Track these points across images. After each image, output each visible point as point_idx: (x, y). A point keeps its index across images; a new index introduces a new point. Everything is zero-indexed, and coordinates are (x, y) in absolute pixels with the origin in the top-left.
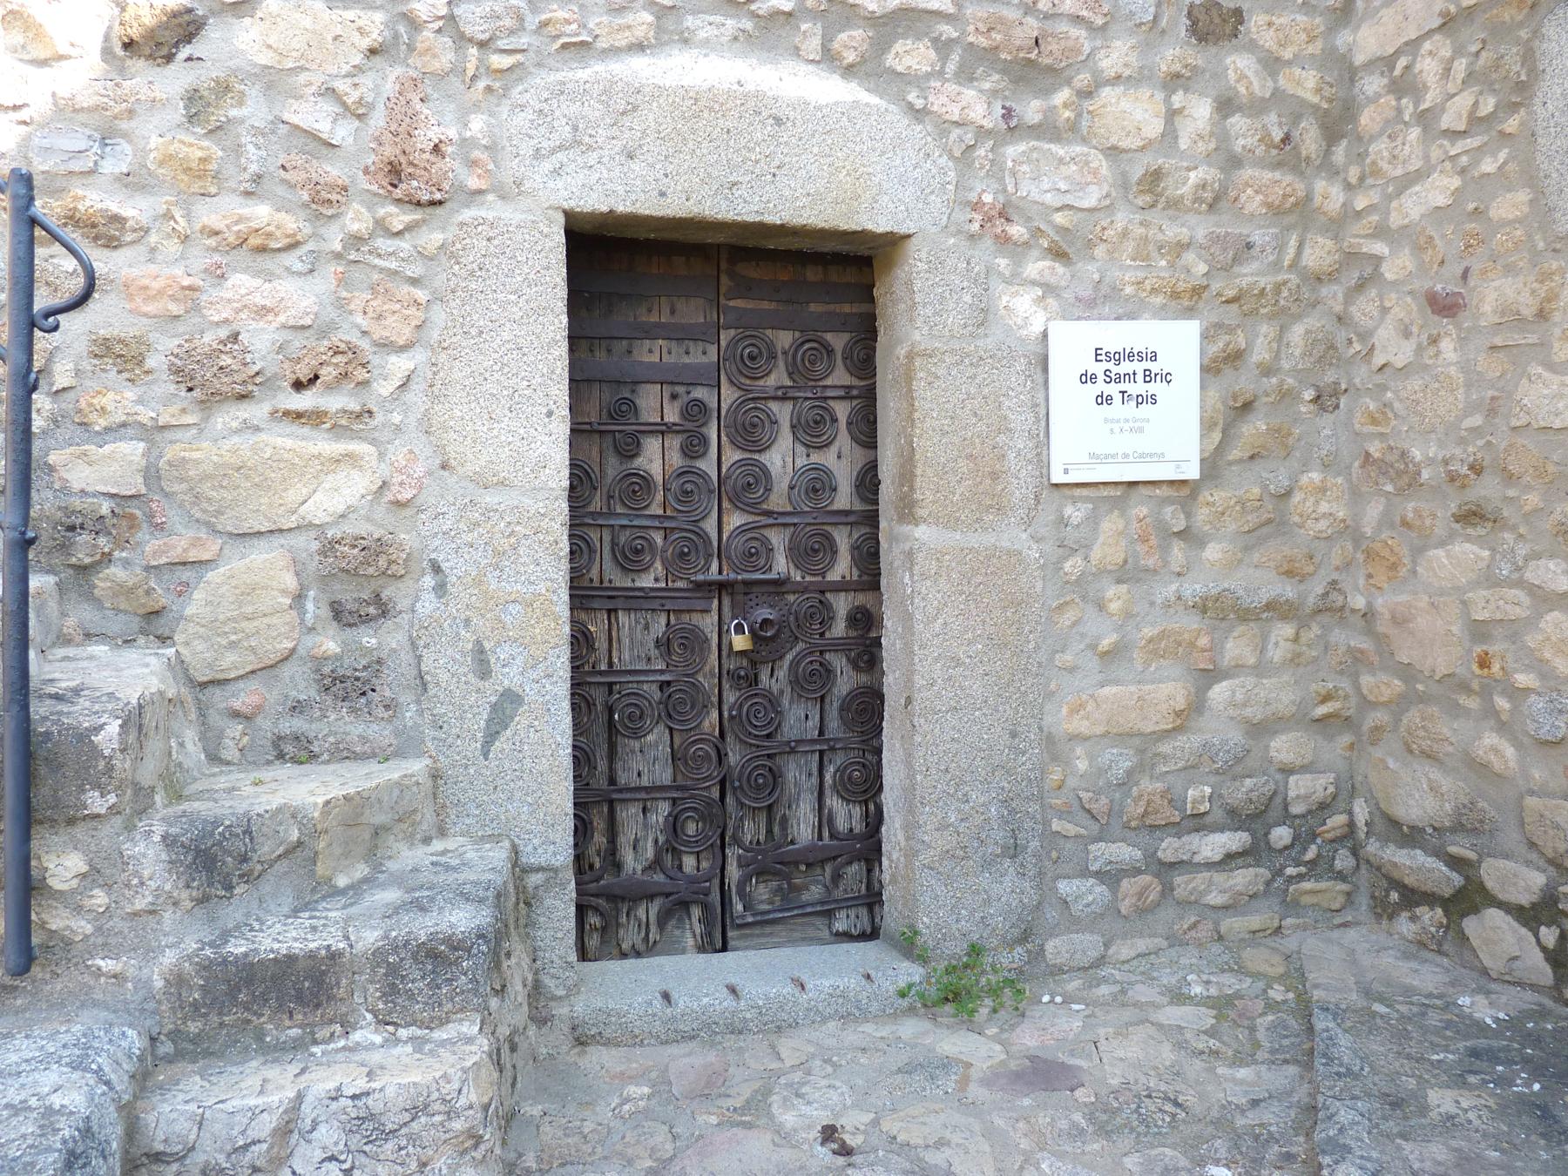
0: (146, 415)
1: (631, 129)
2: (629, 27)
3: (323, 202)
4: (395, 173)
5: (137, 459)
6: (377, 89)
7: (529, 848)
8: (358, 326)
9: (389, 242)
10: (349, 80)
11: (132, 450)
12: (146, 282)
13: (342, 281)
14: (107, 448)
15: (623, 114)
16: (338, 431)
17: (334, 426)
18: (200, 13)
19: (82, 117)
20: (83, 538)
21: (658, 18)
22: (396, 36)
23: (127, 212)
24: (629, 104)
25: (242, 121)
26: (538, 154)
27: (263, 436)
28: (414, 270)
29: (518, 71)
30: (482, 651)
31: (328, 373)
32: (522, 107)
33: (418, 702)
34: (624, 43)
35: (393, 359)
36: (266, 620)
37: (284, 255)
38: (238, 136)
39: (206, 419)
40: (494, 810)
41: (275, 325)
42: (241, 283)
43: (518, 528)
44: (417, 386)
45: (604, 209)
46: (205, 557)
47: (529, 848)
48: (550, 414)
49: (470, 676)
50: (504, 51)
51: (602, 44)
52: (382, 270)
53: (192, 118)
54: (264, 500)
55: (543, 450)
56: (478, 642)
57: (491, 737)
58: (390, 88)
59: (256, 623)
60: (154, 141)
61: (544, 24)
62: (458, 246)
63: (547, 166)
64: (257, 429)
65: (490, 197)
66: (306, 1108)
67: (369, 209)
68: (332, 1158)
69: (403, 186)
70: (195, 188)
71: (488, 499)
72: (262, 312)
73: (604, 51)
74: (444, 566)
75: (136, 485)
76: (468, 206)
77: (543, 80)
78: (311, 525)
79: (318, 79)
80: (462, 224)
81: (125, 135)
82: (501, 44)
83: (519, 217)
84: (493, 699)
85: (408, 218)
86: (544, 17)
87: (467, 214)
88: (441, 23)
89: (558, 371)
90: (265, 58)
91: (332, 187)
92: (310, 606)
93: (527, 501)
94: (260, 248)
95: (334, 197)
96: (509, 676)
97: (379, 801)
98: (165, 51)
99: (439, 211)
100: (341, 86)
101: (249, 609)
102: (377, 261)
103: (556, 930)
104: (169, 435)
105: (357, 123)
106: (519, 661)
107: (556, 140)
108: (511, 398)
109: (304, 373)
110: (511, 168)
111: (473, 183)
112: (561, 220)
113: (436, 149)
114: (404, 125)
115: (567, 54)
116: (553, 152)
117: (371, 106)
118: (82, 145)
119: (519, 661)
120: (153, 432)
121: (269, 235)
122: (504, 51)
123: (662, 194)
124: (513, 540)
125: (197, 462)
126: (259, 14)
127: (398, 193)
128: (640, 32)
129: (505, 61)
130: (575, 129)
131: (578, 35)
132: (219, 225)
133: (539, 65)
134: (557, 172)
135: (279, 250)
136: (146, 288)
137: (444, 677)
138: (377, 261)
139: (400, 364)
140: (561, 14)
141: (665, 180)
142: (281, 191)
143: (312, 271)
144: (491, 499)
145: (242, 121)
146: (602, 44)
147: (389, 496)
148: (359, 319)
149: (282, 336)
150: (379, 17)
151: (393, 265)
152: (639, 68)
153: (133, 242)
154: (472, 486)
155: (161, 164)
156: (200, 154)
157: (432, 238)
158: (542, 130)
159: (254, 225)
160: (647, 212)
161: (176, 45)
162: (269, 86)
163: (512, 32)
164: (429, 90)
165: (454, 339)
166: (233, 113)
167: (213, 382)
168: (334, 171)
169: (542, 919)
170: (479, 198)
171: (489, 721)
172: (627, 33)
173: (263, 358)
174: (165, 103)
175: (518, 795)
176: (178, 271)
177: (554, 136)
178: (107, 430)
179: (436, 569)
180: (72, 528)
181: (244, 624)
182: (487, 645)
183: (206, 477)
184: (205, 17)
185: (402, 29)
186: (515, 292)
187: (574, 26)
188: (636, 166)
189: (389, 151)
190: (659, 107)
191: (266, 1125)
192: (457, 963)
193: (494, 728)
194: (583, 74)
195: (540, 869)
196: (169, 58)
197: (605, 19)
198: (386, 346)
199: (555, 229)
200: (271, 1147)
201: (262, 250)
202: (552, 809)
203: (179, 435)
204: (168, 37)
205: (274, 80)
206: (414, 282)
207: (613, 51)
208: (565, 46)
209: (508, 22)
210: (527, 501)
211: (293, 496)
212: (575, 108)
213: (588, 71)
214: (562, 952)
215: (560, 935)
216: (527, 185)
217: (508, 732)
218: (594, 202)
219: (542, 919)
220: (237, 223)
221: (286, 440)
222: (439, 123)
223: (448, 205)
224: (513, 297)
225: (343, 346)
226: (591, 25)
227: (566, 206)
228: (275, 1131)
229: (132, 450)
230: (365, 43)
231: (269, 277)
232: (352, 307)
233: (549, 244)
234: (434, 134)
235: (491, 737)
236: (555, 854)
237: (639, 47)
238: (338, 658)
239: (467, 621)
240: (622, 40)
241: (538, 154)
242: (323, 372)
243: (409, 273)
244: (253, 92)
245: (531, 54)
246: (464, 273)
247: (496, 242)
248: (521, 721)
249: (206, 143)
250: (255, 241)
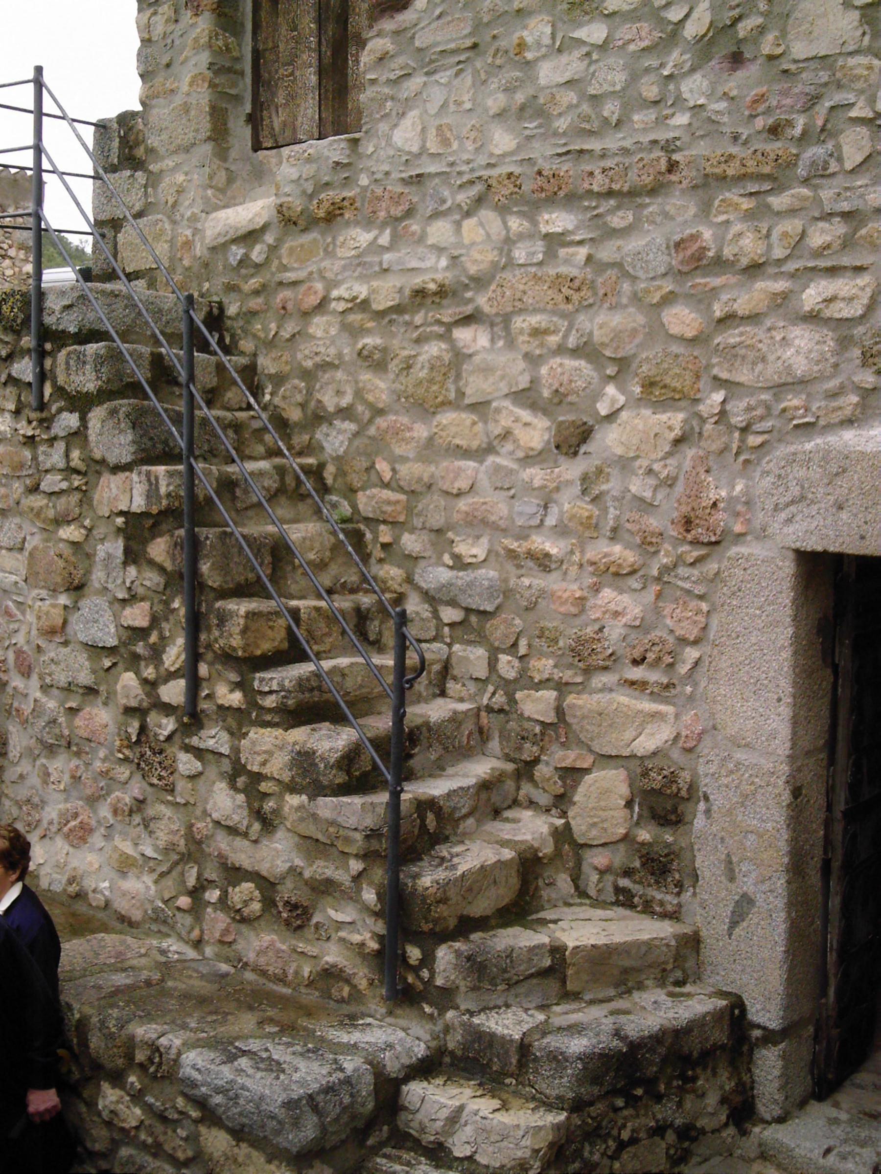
0: (557, 674)
1: (841, 487)
2: (840, 408)
3: (648, 544)
4: (688, 523)
5: (552, 701)
6: (679, 467)
7: (753, 1010)
8: (668, 626)
9: (686, 570)
10: (662, 463)
11: (550, 695)
12: (559, 593)
13: (659, 596)
14: (540, 693)
15: (837, 474)
16: (654, 696)
17: (652, 693)
18: (591, 423)
19: (536, 492)
20: (527, 745)
21: (863, 398)
22: (692, 428)
23: (554, 551)
24: (841, 466)
25: (608, 492)
26: (776, 508)
27: (614, 695)
28: (699, 590)
29: (767, 446)
30: (730, 862)
31: (651, 656)
32: (768, 473)
33: (694, 887)
34: (837, 420)
35: (688, 649)
36: (611, 813)
37: (629, 577)
38: (606, 502)
39: (589, 679)
40: (733, 975)
41: (622, 623)
42: (607, 593)
43: (757, 780)
44: (703, 669)
45: (820, 549)
46: (585, 766)
47: (753, 1010)
48: (779, 700)
49: (723, 878)
50: (758, 433)
51: (822, 422)
52: (682, 589)
53: (584, 492)
54: (614, 735)
55: (774, 725)
56: (728, 855)
57: (734, 924)
58: (687, 464)
59: (606, 813)
60: (566, 506)
61: (784, 410)
62: (726, 574)
63: (783, 516)
64: (611, 690)
65: (749, 538)
66: (464, 1114)
67: (674, 548)
68: (468, 1143)
69: (693, 532)
70: (587, 534)
71: (739, 756)
72: (616, 614)
73: (824, 427)
74: (711, 797)
75: (551, 718)
76: (736, 545)
77: (782, 451)
78: (635, 756)
79: (645, 463)
80: (729, 558)
81: (556, 502)
82: (757, 427)
83: (765, 553)
84: (737, 898)
85: (695, 554)
86: (783, 406)
87: (734, 551)
88: (716, 418)
89: (785, 669)
90: (619, 451)
91: (653, 534)
92: (636, 809)
93: (763, 761)
94: (614, 575)
95: (654, 540)
96: (748, 884)
97: (628, 952)
98: (572, 450)
99: (717, 548)
100: (656, 467)
101: (603, 804)
102: (680, 583)
103: (768, 1073)
104: (569, 688)
105: (668, 490)
106: (753, 875)
107: (788, 499)
108: (755, 684)
109: (637, 654)
110: (760, 518)
111: (738, 528)
112: (791, 555)
113: (715, 504)
114: (696, 490)
115: (799, 432)
116: (787, 505)
117: (675, 479)
118: (534, 510)
119: (753, 875)
120: (562, 687)
121: (620, 565)
122: (758, 433)
123: (863, 538)
124: (753, 788)
125: (581, 707)
126: (619, 421)
127: (689, 537)
128: (848, 411)
129: (759, 440)
130: (803, 487)
131: (805, 417)
132: (596, 559)
133: (780, 440)
134: (789, 521)
135: (626, 574)
136: (560, 597)
137: (707, 874)
138: (680, 583)
139: (691, 654)
140: (795, 402)
141: (866, 527)
142: (627, 536)
143: (643, 588)
144: (740, 755)
145: (608, 492)
146: (822, 422)
147: (680, 744)
148: (668, 621)
149: (623, 631)
150: (681, 416)
151: (687, 585)
152: (849, 438)
153: (556, 569)
154: (730, 744)
155: (570, 520)
156: (586, 514)
157: (712, 566)
158: (781, 489)
159: (612, 559)
160: (851, 552)
161: (578, 446)
162: (623, 468)
163: (762, 418)
164: (711, 464)
165: (723, 639)
166: (604, 487)
167: (587, 659)
168: (653, 523)
169: (760, 1062)
170: (742, 539)
171: (733, 912)
172: (839, 413)
173: (615, 644)
174: (569, 483)
175: (749, 970)
176: (575, 587)
177: (789, 494)
178: (541, 682)
179: (706, 798)
180: (523, 738)
181: (601, 813)
182: (735, 859)
183: (584, 717)
184: (592, 426)
185: (695, 423)
186: (760, 608)
187: (801, 412)
188: (844, 515)
189: (685, 509)
190: (862, 468)
191: (444, 1114)
192: (565, 1068)
193: (736, 918)
194: (809, 446)
195: (759, 1026)
196: (576, 454)
197: (823, 403)
198: (683, 641)
199: (787, 564)
200: (444, 1126)
201: (617, 574)
202: (769, 987)
203: (574, 688)
204: (574, 441)
205: (625, 464)
206: (701, 597)
207: (829, 427)
208: (797, 426)
209: (759, 412)
210: (763, 761)
211: (629, 735)
212: (802, 473)
213: (813, 443)
214: (770, 1090)
215: (770, 1077)
216: (770, 531)
217: (745, 924)
218: (814, 544)
219: (760, 1062)
220: (604, 557)
221: (624, 699)
222: (717, 490)
223: (723, 544)
224: (758, 612)
225: (657, 640)
226: (814, 409)
227: (793, 546)
228: (447, 1119)
229: (550, 695)
230: (672, 436)
231: (621, 592)
232: (665, 613)
233: (782, 574)
234: (713, 496)
235: (734, 924)
236: (770, 1020)
237: (849, 422)
238: (650, 844)
239: (722, 839)
240: (836, 418)
241: (776, 508)
242: (648, 656)
243: (696, 592)
244: (615, 472)
245: (775, 433)
246: (729, 593)
247: (749, 572)
248: (753, 918)
249: (590, 507)
250: (612, 569)
